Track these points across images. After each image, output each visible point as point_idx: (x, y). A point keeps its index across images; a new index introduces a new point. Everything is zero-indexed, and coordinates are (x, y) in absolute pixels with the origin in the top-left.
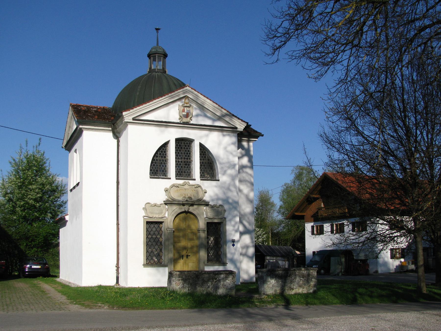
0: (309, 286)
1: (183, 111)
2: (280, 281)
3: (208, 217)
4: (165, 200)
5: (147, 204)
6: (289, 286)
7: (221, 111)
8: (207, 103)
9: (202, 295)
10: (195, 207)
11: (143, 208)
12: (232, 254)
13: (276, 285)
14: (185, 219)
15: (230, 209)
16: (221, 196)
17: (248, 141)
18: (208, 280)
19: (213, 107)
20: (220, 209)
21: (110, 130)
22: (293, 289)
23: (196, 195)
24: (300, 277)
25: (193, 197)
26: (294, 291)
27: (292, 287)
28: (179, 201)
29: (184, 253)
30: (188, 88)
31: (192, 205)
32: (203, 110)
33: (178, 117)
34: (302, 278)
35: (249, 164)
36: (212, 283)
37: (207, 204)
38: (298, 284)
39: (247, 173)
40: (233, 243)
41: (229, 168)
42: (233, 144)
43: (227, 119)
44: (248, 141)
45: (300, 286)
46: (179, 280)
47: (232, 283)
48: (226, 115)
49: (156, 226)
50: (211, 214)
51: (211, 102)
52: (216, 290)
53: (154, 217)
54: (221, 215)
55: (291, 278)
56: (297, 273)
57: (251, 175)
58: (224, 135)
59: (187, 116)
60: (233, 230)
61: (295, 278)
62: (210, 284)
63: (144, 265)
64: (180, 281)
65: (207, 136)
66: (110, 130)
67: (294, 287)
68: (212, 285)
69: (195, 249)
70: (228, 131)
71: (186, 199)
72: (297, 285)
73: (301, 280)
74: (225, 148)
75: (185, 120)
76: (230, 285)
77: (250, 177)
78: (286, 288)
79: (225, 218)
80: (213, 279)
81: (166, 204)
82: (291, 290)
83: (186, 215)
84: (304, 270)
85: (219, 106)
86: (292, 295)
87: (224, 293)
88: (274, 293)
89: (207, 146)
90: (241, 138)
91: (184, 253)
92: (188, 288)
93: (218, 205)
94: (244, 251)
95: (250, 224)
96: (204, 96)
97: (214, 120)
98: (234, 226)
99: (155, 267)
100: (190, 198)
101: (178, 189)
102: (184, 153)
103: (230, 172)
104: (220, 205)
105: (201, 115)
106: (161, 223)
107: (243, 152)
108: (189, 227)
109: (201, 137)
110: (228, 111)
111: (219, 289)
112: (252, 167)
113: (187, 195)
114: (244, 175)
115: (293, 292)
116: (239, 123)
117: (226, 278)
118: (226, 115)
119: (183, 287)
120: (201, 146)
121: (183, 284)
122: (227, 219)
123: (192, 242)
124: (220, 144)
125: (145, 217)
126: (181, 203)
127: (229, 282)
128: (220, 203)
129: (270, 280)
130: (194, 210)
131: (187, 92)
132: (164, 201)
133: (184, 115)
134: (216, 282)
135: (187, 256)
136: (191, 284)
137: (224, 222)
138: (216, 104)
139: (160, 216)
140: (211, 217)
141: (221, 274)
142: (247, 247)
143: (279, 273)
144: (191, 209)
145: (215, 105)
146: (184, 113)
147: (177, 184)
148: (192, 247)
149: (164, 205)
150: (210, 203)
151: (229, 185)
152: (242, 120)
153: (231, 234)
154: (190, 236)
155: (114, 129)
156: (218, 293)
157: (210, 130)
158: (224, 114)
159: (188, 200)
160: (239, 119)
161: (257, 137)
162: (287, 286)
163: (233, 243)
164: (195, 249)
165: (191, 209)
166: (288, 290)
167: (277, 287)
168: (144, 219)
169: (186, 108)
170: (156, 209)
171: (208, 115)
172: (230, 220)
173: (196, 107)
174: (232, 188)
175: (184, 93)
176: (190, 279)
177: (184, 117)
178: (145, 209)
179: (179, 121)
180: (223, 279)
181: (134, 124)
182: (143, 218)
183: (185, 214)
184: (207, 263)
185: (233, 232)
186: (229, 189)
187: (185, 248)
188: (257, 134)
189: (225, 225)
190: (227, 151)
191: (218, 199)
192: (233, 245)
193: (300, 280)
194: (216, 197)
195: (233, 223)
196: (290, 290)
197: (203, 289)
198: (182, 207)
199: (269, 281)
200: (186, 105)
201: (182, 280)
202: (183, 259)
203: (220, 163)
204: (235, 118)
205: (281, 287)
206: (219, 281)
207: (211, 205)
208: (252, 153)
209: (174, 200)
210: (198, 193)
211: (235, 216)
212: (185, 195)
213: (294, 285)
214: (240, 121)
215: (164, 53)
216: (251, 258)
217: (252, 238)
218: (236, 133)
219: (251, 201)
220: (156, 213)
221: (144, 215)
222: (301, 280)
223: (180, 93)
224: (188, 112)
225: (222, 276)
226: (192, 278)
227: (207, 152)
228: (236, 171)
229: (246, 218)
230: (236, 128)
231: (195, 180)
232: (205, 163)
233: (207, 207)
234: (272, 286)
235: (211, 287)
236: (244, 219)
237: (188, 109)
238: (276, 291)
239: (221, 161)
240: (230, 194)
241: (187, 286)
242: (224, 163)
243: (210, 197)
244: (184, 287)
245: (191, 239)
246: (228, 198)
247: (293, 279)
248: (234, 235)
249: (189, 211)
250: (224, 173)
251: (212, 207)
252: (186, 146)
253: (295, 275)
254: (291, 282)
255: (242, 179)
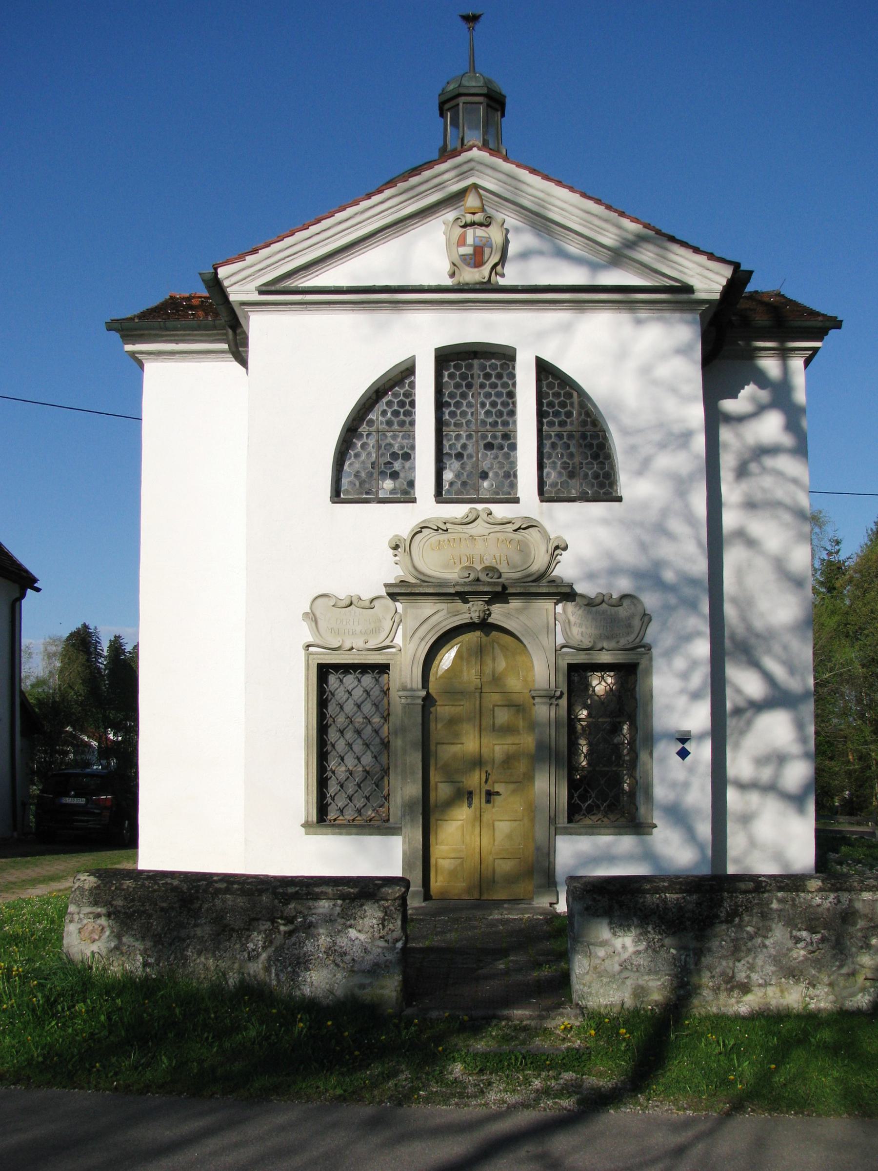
0: (853, 974)
1: (462, 242)
2: (667, 941)
3: (573, 643)
4: (392, 581)
5: (320, 600)
6: (723, 974)
7: (620, 227)
8: (530, 190)
9: (217, 992)
10: (515, 604)
11: (306, 614)
12: (673, 785)
13: (641, 961)
14: (480, 652)
15: (668, 609)
16: (629, 556)
17: (784, 354)
18: (250, 924)
19: (585, 216)
20: (622, 612)
21: (222, 352)
22: (745, 988)
23: (516, 558)
24: (790, 923)
25: (503, 568)
26: (749, 998)
27: (741, 976)
28: (443, 583)
29: (474, 780)
30: (475, 153)
31: (501, 595)
32: (550, 233)
33: (447, 267)
34: (804, 934)
35: (787, 440)
36: (268, 942)
37: (567, 595)
38: (776, 960)
39: (779, 474)
40: (680, 746)
41: (663, 446)
42: (682, 351)
43: (647, 254)
44: (784, 354)
45: (792, 973)
46: (98, 916)
47: (382, 943)
48: (639, 240)
49: (368, 680)
50: (583, 629)
51: (575, 198)
52: (294, 975)
53: (347, 646)
54: (628, 634)
55: (740, 927)
56: (775, 905)
57: (795, 481)
58: (639, 322)
59: (477, 258)
60: (682, 691)
61: (764, 931)
62: (257, 939)
63: (307, 825)
64: (103, 921)
65: (567, 328)
66: (222, 352)
67: (754, 976)
68: (271, 950)
69: (522, 767)
70: (659, 306)
71: (472, 577)
72: (770, 969)
73: (798, 940)
74: (645, 371)
75: (471, 275)
76: (366, 951)
77: (792, 488)
78: (706, 980)
79: (649, 648)
80: (273, 921)
81: (393, 596)
82: (735, 993)
83: (484, 638)
84: (820, 890)
85: (609, 207)
86: (738, 1017)
87: (339, 992)
88: (629, 1003)
89: (566, 366)
90: (749, 345)
91: (474, 780)
92: (144, 953)
93: (615, 596)
94: (766, 774)
95: (792, 670)
96: (546, 178)
97: (595, 267)
98: (685, 676)
99: (350, 834)
100: (490, 570)
101: (446, 536)
102: (483, 405)
103: (666, 461)
104: (624, 597)
105: (540, 253)
106: (384, 668)
107: (764, 395)
108: (497, 680)
109: (541, 335)
110: (647, 226)
111: (307, 969)
112: (801, 450)
113: (482, 561)
114: (767, 481)
115: (745, 1004)
116: (700, 270)
117: (347, 917)
118: (639, 240)
119: (117, 948)
120: (544, 369)
121: (119, 937)
122: (655, 652)
123: (510, 740)
124: (622, 354)
125: (311, 649)
126: (452, 591)
127: (362, 937)
128: (624, 585)
129: (605, 933)
130: (508, 615)
131: (471, 170)
132: (386, 585)
133: (464, 258)
134: (290, 933)
135: (490, 795)
136: (157, 940)
137: (643, 663)
138: (598, 201)
139: (372, 644)
140: (587, 643)
141: (317, 897)
142: (780, 759)
143: (664, 901)
144: (498, 614)
145: (590, 205)
146: (463, 250)
147: (437, 519)
148: (509, 760)
149: (389, 601)
150: (579, 589)
151: (665, 512)
152: (711, 256)
153: (669, 708)
154: (503, 716)
155: (237, 346)
156: (307, 991)
157: (580, 306)
158: (631, 237)
159: (483, 577)
160: (697, 250)
161: (819, 333)
162: (710, 968)
163: (680, 746)
164: (522, 767)
165: (498, 614)
166: (716, 990)
167: (650, 972)
168: (308, 655)
169: (470, 232)
170: (356, 618)
171: (573, 248)
172: (669, 653)
173: (520, 224)
174: (676, 525)
175: (462, 175)
176: (150, 916)
177: (468, 265)
178: (312, 617)
179: (448, 282)
180: (329, 920)
181: (264, 308)
182: (303, 652)
183: (478, 633)
184: (570, 821)
185: (682, 701)
186: (661, 529)
187: (478, 762)
188: (817, 323)
189: (649, 672)
190: (655, 383)
191: (614, 571)
192: (683, 754)
193: (790, 944)
194: (604, 564)
195: (680, 663)
196: (731, 990)
197: (222, 965)
198: (459, 605)
199: (604, 944)
200: (469, 218)
201: (109, 915)
202: (470, 805)
203: (625, 432)
204: (682, 251)
205: (676, 976)
206: (309, 928)
207: (582, 596)
208: (800, 396)
209: (424, 579)
210: (523, 549)
211: (688, 637)
212: (470, 559)
213: (752, 968)
214: (702, 259)
215: (485, 91)
216: (796, 800)
217: (800, 726)
218: (692, 310)
219: (797, 582)
220: (354, 633)
221: (310, 639)
222: (798, 940)
223: (446, 177)
224: (478, 243)
225: (324, 906)
226: (162, 909)
227: (575, 394)
228: (697, 457)
229: (777, 648)
230: (688, 289)
231: (516, 501)
232: (571, 436)
233: (570, 606)
234: (617, 968)
235: (264, 956)
236: (769, 651)
237: (480, 232)
238: (640, 992)
239: (627, 421)
240: (665, 550)
241: (139, 945)
242: (639, 431)
243: (581, 561)
244: (124, 949)
245: (507, 730)
246: (658, 565)
247: (751, 938)
248: (685, 713)
249: (490, 620)
250: (644, 467)
251: (590, 604)
252: (487, 376)
253: (765, 916)
254: (736, 951)
255: (759, 496)
